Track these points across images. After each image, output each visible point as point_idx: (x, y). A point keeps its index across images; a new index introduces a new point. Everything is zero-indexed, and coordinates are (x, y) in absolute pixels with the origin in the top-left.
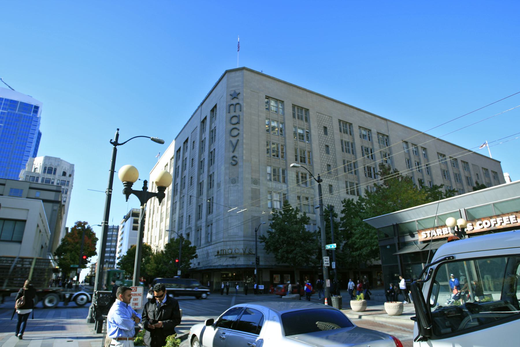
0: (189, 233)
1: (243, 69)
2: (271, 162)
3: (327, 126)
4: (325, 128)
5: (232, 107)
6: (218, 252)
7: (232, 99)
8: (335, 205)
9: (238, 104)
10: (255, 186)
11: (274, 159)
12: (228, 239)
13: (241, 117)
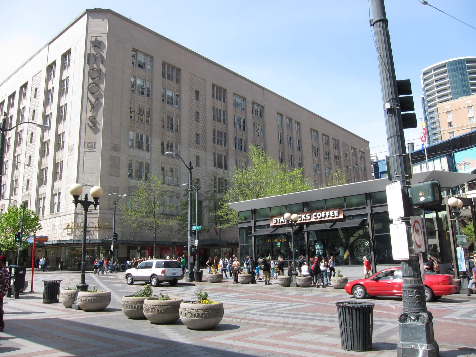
1: (108, 12)
2: (134, 127)
3: (199, 90)
4: (197, 92)
6: (68, 225)
10: (115, 152)
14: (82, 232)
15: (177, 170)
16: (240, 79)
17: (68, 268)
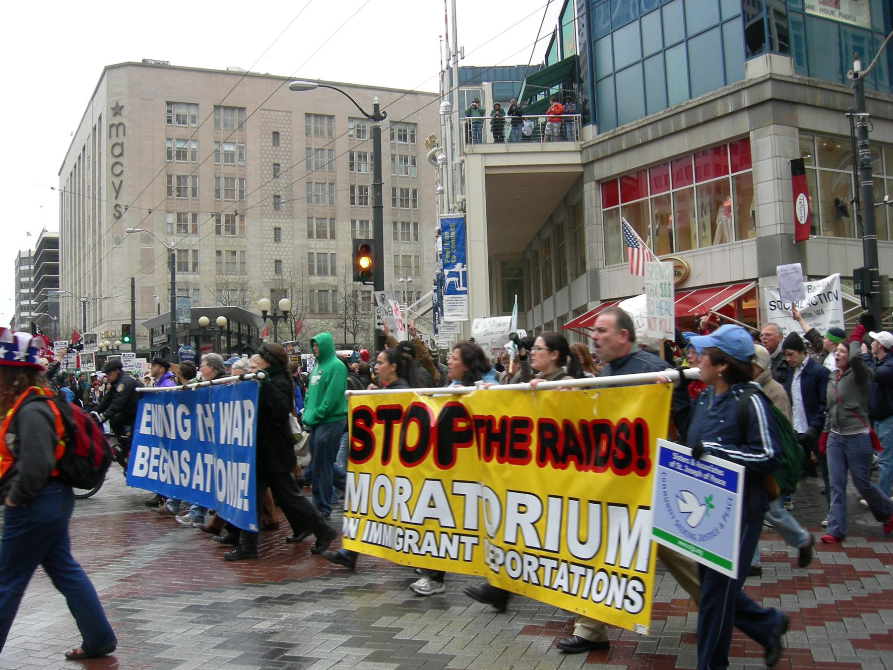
0: (748, 133)
3: (280, 130)
4: (276, 134)
5: (114, 130)
7: (114, 115)
8: (282, 258)
9: (120, 124)
11: (178, 201)
12: (113, 319)
13: (125, 145)
14: (138, 336)
15: (243, 252)
16: (364, 91)
17: (821, 572)
